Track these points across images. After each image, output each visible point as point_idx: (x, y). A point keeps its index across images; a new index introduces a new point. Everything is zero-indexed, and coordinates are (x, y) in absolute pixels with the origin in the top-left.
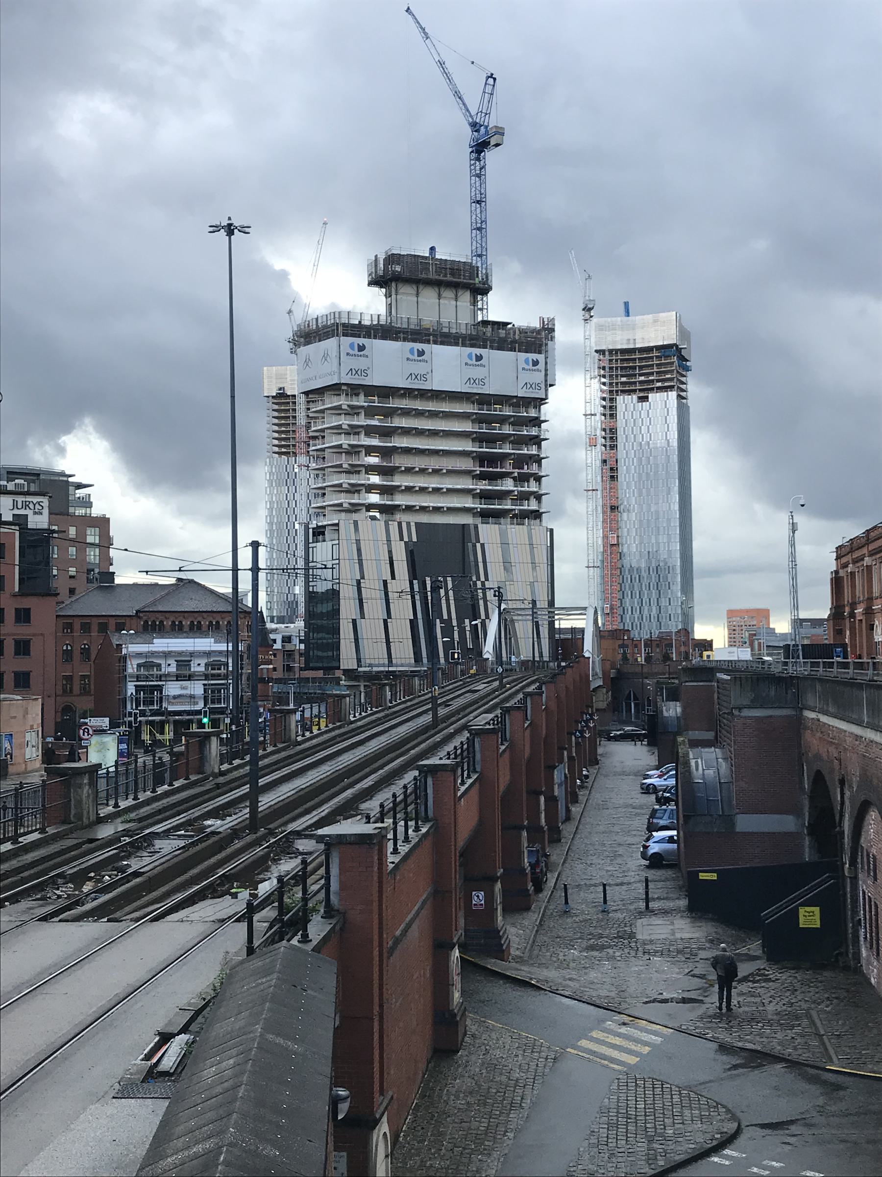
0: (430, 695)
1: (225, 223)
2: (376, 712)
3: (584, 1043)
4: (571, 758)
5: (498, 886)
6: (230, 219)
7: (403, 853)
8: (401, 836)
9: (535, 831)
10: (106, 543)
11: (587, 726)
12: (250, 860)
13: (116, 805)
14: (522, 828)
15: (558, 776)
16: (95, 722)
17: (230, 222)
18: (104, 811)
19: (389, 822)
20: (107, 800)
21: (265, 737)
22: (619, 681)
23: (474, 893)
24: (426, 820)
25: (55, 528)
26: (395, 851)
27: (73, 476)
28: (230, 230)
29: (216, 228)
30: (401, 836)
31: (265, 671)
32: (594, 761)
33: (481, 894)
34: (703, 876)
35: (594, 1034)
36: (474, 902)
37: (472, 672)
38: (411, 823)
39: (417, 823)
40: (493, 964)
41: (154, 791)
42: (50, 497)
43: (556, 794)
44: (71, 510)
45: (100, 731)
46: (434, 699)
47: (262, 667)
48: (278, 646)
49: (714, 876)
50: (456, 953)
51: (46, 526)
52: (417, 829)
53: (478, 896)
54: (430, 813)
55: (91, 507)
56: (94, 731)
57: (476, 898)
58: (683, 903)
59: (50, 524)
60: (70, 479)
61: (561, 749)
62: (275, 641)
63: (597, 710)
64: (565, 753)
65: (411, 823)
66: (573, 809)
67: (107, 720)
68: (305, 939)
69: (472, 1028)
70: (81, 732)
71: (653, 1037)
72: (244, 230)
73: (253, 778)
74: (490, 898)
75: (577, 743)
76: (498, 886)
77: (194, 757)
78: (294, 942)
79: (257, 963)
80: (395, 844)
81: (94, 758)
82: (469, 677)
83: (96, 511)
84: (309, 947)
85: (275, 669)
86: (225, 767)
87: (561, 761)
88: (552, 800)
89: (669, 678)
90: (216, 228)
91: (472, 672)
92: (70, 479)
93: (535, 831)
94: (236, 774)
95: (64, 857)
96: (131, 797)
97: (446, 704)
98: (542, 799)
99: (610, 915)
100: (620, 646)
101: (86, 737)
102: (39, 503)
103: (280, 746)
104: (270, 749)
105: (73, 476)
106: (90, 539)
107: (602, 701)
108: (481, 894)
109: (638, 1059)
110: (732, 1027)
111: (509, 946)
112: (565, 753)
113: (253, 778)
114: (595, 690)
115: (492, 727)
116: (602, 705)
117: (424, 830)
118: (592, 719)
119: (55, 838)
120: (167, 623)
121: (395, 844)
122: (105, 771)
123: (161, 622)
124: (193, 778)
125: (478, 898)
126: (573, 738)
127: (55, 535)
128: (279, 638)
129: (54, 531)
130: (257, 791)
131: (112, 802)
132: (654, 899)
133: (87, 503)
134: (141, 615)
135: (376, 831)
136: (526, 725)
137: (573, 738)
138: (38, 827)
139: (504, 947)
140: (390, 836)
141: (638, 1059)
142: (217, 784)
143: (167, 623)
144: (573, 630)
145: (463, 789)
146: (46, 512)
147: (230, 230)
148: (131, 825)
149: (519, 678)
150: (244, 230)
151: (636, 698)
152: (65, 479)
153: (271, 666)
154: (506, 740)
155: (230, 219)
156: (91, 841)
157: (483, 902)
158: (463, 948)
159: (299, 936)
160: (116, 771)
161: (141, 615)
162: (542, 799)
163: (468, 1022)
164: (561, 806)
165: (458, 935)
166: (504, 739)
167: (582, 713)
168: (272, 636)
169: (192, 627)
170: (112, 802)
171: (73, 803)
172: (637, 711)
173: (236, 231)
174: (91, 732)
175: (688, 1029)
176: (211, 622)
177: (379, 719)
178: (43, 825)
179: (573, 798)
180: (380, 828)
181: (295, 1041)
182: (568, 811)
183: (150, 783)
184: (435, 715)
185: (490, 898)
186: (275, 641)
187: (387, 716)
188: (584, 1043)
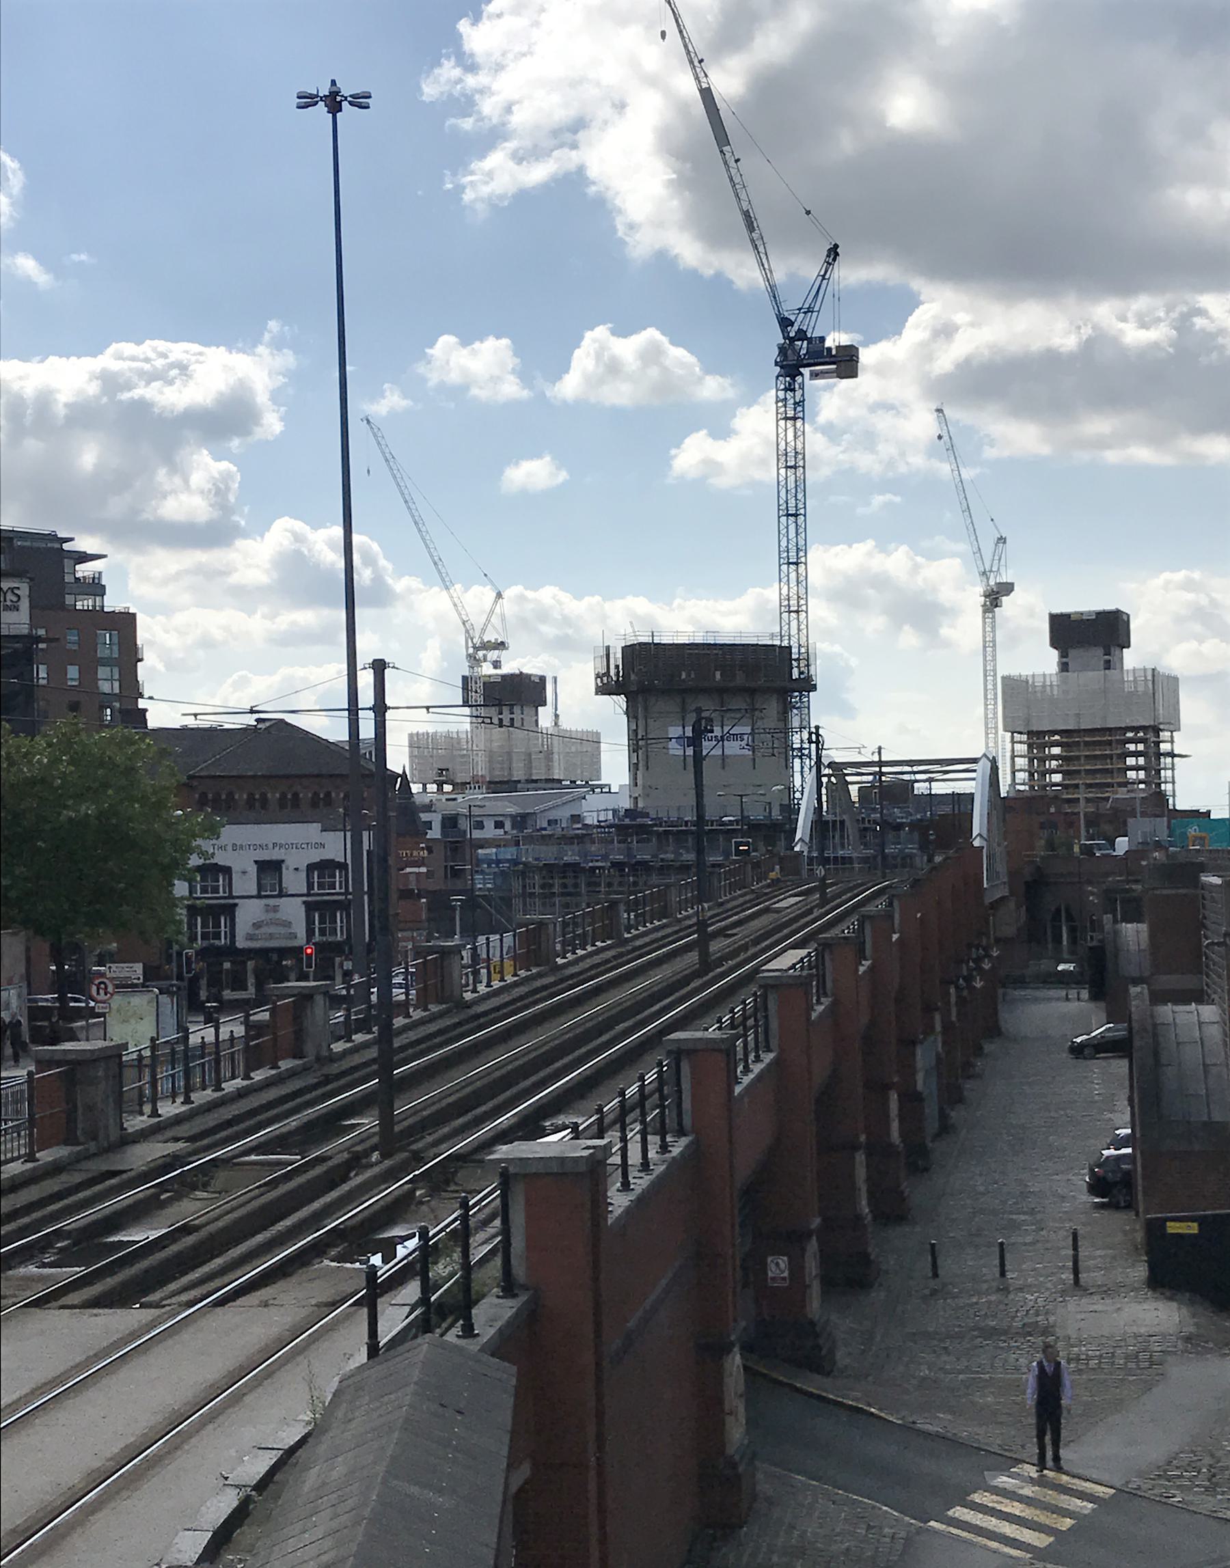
0: (694, 920)
1: (325, 91)
2: (603, 949)
3: (959, 1512)
4: (947, 1027)
5: (813, 1246)
6: (333, 82)
7: (638, 1190)
8: (635, 1157)
9: (879, 1150)
10: (130, 655)
11: (979, 969)
12: (381, 1203)
13: (155, 1113)
14: (855, 1148)
15: (924, 1057)
16: (117, 970)
17: (334, 89)
18: (136, 1123)
19: (613, 1136)
20: (141, 1105)
21: (407, 994)
22: (1033, 887)
23: (769, 1259)
24: (681, 1132)
25: (42, 632)
26: (626, 1186)
27: (72, 539)
28: (334, 102)
29: (307, 100)
30: (635, 1157)
31: (412, 878)
32: (994, 1030)
33: (783, 1261)
34: (1173, 1228)
35: (977, 1497)
36: (770, 1274)
37: (772, 875)
38: (654, 1140)
39: (663, 1139)
40: (812, 1384)
41: (218, 1088)
42: (31, 579)
43: (920, 1087)
44: (69, 599)
45: (125, 986)
46: (702, 925)
47: (408, 870)
48: (435, 833)
49: (1193, 1228)
50: (736, 1360)
51: (25, 630)
52: (664, 1148)
53: (777, 1264)
54: (687, 1121)
55: (103, 595)
56: (117, 987)
57: (773, 1267)
58: (1140, 1272)
59: (31, 627)
60: (66, 546)
61: (928, 1009)
62: (429, 825)
63: (998, 941)
64: (937, 1017)
65: (654, 1140)
66: (953, 1114)
67: (139, 968)
68: (468, 1331)
69: (765, 1487)
70: (94, 988)
71: (1079, 1502)
72: (360, 101)
73: (385, 1064)
74: (797, 1269)
75: (961, 1001)
76: (813, 1246)
77: (285, 1032)
78: (451, 1337)
79: (379, 1370)
80: (625, 1175)
81: (118, 1032)
82: (768, 886)
83: (112, 602)
84: (473, 1346)
85: (429, 874)
86: (338, 1047)
87: (929, 1030)
88: (912, 1099)
89: (1128, 882)
90: (307, 100)
91: (772, 875)
92: (66, 546)
93: (879, 1150)
94: (357, 1059)
95: (66, 1202)
96: (180, 1100)
97: (722, 933)
98: (894, 1096)
99: (1011, 1296)
100: (1042, 826)
101: (102, 997)
102: (12, 589)
103: (434, 1008)
104: (417, 1014)
105: (72, 539)
106: (102, 652)
107: (1010, 921)
108: (783, 1261)
109: (1052, 1539)
110: (1217, 1485)
111: (832, 1352)
112: (937, 1017)
113: (385, 1064)
114: (995, 906)
115: (797, 973)
116: (1009, 931)
117: (676, 1151)
118: (988, 956)
119: (56, 1168)
120: (241, 796)
121: (625, 1175)
122: (135, 1056)
123: (230, 794)
124: (285, 1065)
125: (778, 1267)
126: (952, 990)
127: (42, 646)
128: (436, 820)
129: (39, 639)
130: (393, 1088)
131: (147, 1109)
132: (1088, 1270)
133: (96, 587)
134: (195, 783)
135: (586, 1153)
136: (862, 969)
137: (952, 990)
138: (23, 1152)
139: (824, 1352)
140: (617, 1159)
141: (1052, 1539)
142: (327, 1076)
143: (241, 796)
144: (956, 798)
145: (746, 1080)
146: (25, 605)
147: (334, 102)
148: (181, 1145)
149: (861, 885)
150: (360, 101)
151: (1070, 918)
152: (57, 546)
153: (423, 870)
154: (825, 995)
155: (333, 82)
156: (114, 1174)
157: (786, 1274)
158: (747, 1349)
159: (457, 1330)
160: (153, 1056)
161: (195, 783)
162: (894, 1096)
163: (760, 1476)
164: (931, 1109)
165: (738, 1329)
166: (822, 991)
167: (970, 946)
168: (424, 817)
169: (282, 803)
170: (147, 1109)
171: (80, 1112)
172: (1073, 940)
173: (345, 104)
174: (110, 989)
175: (1139, 1488)
176: (316, 794)
177: (607, 961)
178: (31, 1148)
179: (953, 1096)
180: (594, 1147)
181: (441, 1491)
182: (943, 1116)
183: (241, 1069)
184: (704, 954)
185: (797, 1269)
186: (429, 825)
187: (621, 955)
188: (959, 1512)
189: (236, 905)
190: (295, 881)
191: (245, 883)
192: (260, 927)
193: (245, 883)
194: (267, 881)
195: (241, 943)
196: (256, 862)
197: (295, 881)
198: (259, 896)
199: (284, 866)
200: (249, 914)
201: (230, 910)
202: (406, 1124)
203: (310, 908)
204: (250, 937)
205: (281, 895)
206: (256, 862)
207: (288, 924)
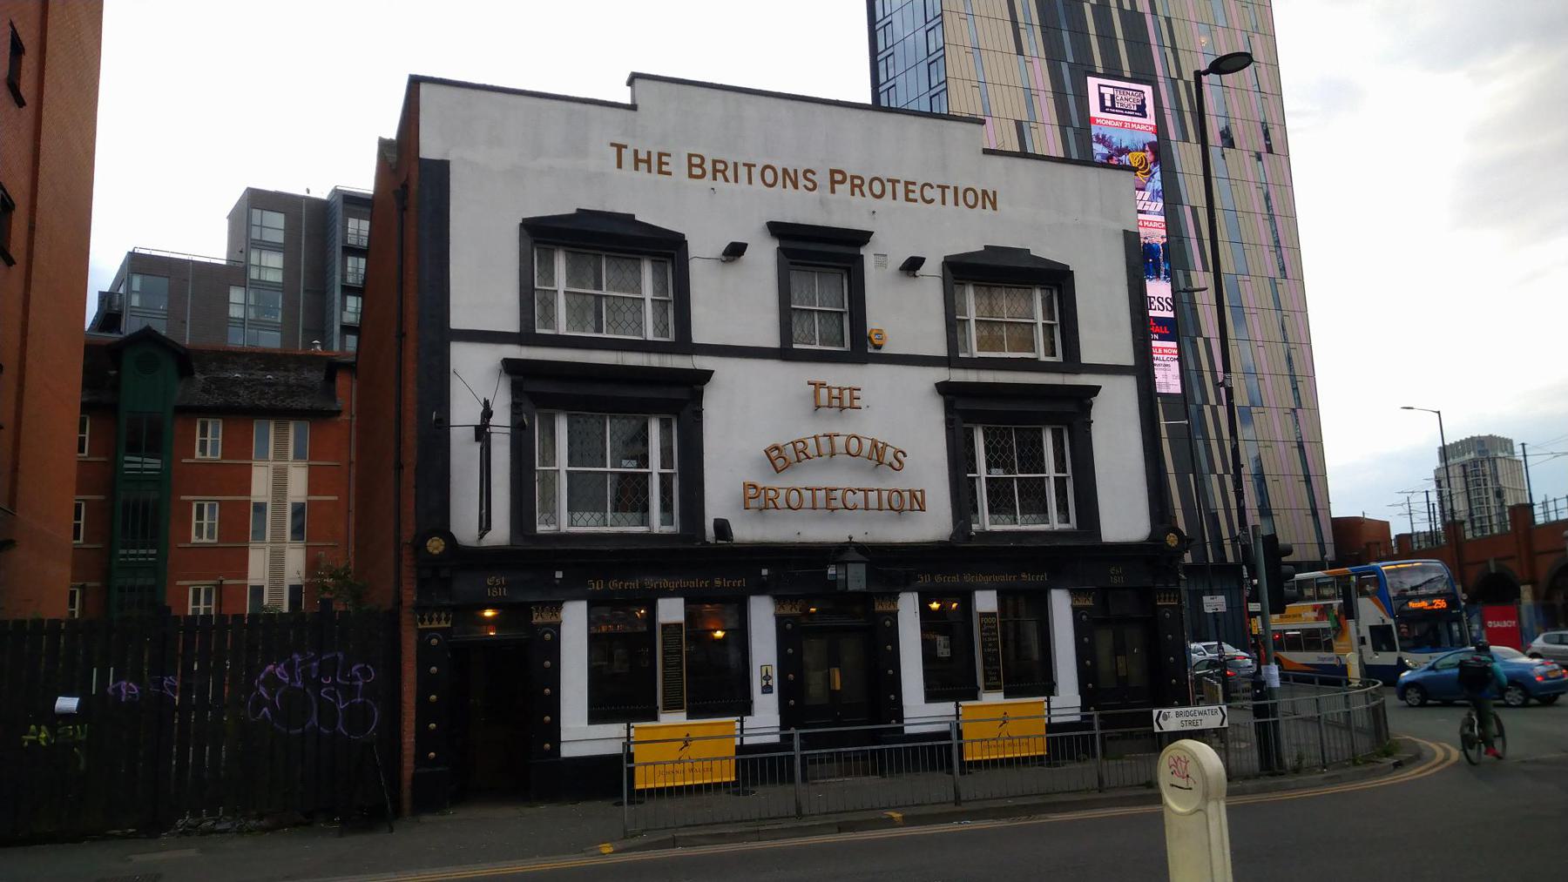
189: (706, 375)
199: (868, 253)
201: (681, 398)
202: (683, 583)
203: (962, 406)
207: (880, 457)
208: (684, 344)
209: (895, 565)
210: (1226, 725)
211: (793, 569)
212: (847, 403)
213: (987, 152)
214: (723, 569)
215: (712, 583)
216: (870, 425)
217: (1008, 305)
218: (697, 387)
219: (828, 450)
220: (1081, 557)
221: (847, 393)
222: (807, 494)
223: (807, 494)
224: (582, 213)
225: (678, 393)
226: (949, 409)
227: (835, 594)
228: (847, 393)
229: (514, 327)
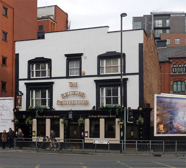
33: (110, 117)
108: (110, 117)
134: (171, 61)
161: (171, 61)
189: (53, 83)
190: (89, 65)
191: (59, 67)
192: (67, 96)
193: (59, 67)
194: (74, 65)
195: (56, 107)
196: (66, 55)
197: (89, 65)
198: (68, 77)
199: (83, 57)
200: (60, 88)
201: (49, 86)
202: (49, 117)
203: (99, 84)
204: (60, 103)
205: (80, 76)
206: (66, 55)
207: (82, 95)
208: (125, 74)
209: (85, 114)
210: (109, 143)
211: (64, 114)
212: (75, 85)
213: (108, 32)
214: (55, 116)
215: (53, 117)
216: (80, 90)
217: (112, 63)
218: (126, 81)
219: (74, 94)
220: (120, 113)
221: (75, 84)
222: (67, 102)
223: (67, 102)
224: (36, 58)
225: (49, 86)
226: (96, 84)
227: (73, 120)
228: (75, 84)
229: (96, 74)
